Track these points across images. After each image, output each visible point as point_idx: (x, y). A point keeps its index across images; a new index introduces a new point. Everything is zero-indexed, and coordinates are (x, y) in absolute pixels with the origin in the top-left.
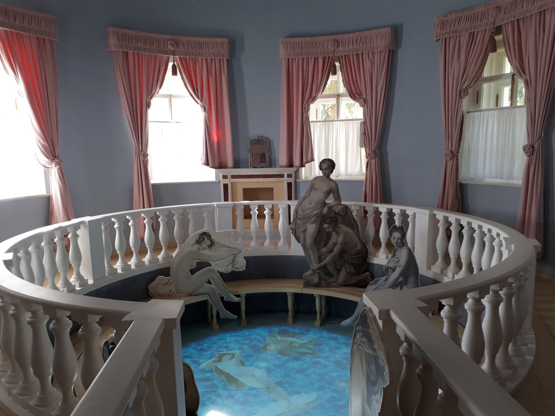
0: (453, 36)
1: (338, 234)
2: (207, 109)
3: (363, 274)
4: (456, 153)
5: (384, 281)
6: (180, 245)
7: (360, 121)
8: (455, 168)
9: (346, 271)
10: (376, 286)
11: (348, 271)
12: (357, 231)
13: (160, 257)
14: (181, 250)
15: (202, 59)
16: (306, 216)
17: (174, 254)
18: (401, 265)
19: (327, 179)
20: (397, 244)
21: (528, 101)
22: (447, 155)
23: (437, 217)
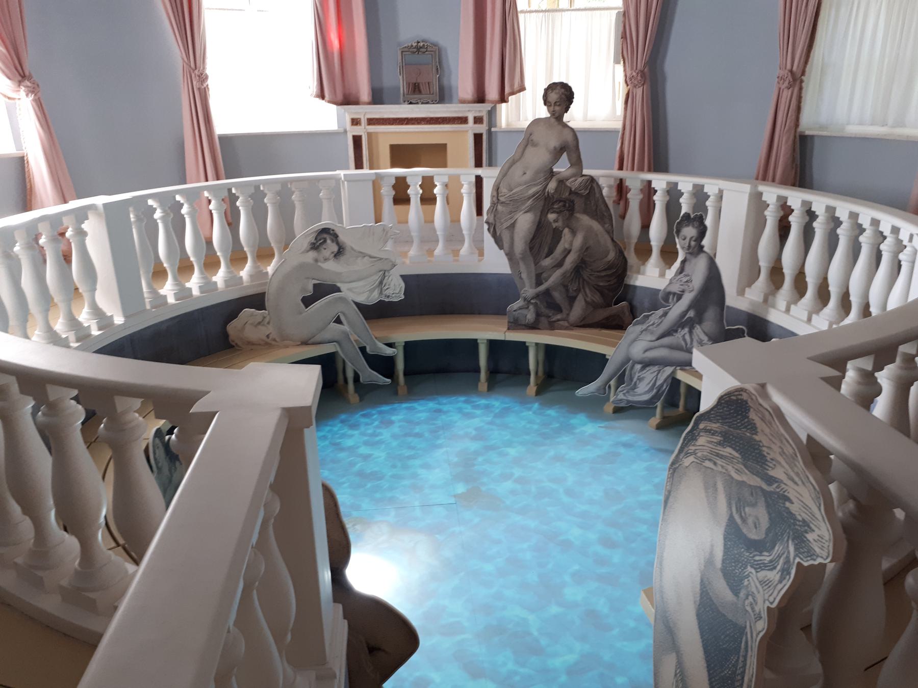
1: (574, 232)
3: (615, 305)
4: (800, 75)
5: (660, 317)
6: (280, 253)
7: (616, 11)
8: (795, 105)
9: (585, 300)
10: (644, 327)
11: (588, 300)
12: (610, 226)
13: (245, 273)
14: (283, 262)
16: (516, 198)
17: (270, 269)
18: (693, 287)
19: (556, 123)
20: (688, 249)
22: (781, 79)
23: (764, 198)
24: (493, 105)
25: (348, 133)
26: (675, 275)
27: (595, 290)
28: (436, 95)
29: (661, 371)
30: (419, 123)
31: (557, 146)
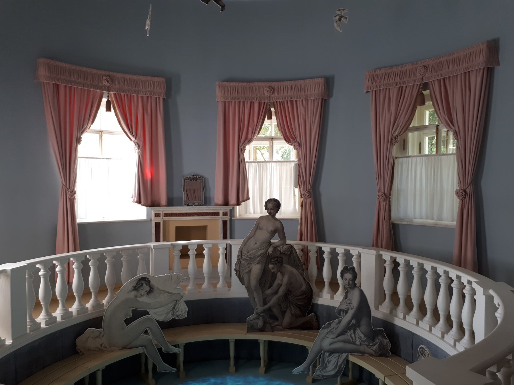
0: (383, 89)
1: (283, 275)
2: (141, 146)
3: (307, 315)
4: (388, 195)
5: (337, 324)
9: (291, 313)
10: (329, 330)
11: (293, 313)
13: (89, 305)
15: (138, 96)
16: (251, 256)
19: (272, 218)
21: (458, 150)
22: (380, 197)
25: (153, 221)
26: (343, 300)
27: (296, 307)
28: (203, 201)
29: (340, 356)
30: (193, 216)
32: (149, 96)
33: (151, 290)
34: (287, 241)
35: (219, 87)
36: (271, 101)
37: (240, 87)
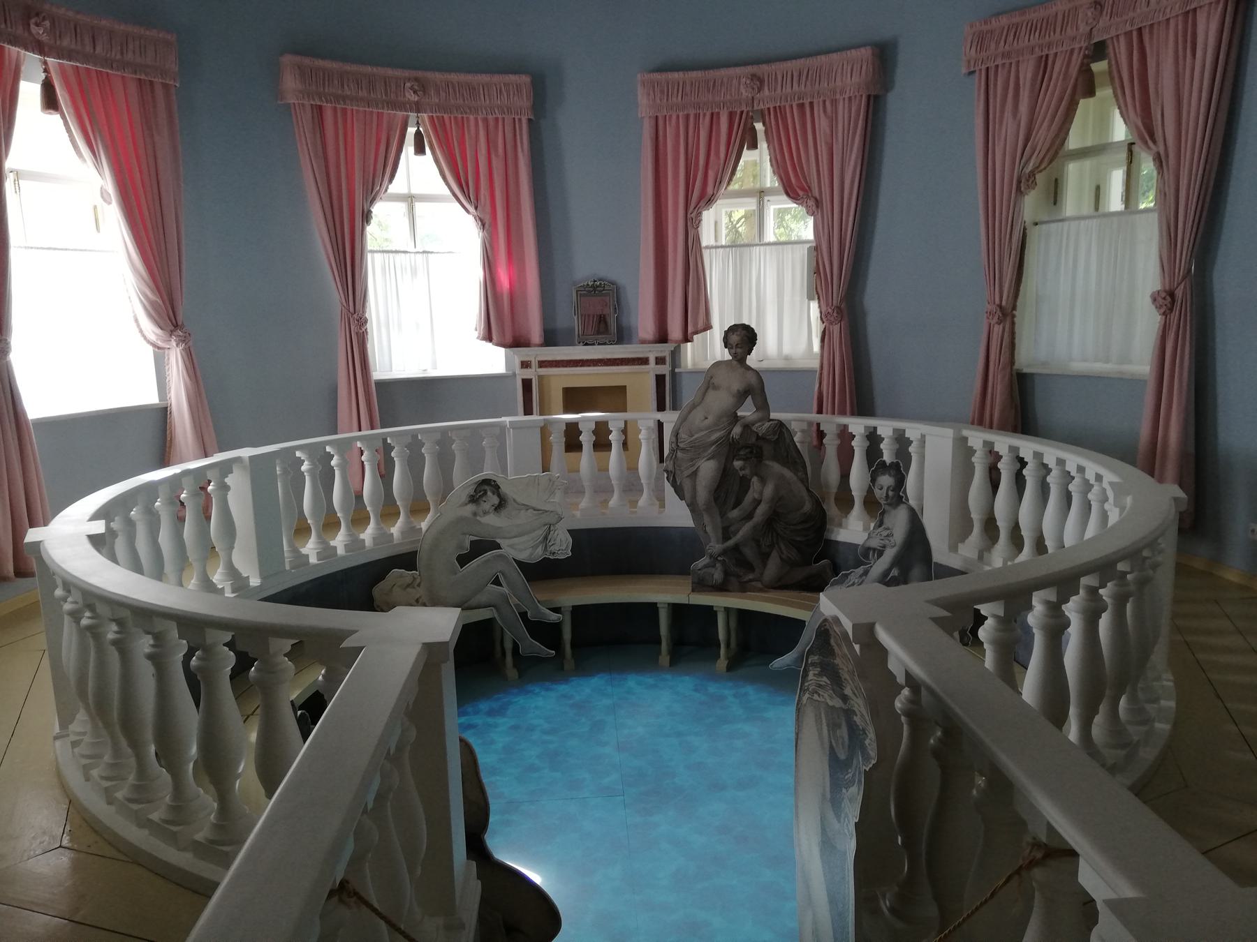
0: (1062, 52)
1: (763, 481)
2: (483, 224)
4: (1010, 310)
5: (861, 576)
9: (781, 558)
11: (784, 556)
13: (396, 530)
15: (476, 119)
17: (424, 525)
19: (739, 366)
24: (677, 345)
30: (594, 365)
31: (741, 389)
32: (500, 116)
33: (501, 505)
34: (771, 414)
35: (644, 85)
36: (756, 108)
37: (687, 82)
